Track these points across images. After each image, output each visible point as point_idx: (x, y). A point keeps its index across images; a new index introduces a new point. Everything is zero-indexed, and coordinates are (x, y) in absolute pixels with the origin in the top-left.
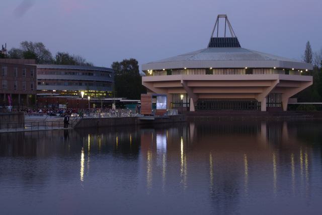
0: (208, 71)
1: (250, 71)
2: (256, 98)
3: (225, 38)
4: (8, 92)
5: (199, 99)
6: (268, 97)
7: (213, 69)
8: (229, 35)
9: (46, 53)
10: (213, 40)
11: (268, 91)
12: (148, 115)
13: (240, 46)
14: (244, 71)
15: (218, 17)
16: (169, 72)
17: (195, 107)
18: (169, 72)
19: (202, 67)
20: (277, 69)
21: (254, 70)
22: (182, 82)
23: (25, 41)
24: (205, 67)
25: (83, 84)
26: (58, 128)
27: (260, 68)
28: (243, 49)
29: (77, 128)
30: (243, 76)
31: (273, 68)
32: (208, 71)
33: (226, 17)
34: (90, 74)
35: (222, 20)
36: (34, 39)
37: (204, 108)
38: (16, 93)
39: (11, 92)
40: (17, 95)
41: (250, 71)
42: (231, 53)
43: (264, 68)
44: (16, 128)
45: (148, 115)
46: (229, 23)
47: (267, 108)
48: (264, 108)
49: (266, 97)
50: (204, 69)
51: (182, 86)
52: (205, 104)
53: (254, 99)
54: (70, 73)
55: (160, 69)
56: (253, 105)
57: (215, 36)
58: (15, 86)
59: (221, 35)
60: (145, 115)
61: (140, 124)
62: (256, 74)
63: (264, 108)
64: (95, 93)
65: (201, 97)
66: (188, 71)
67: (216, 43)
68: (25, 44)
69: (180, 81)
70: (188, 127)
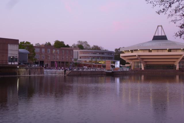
0: (150, 51)
1: (170, 50)
2: (174, 63)
3: (158, 36)
4: (60, 61)
5: (147, 64)
6: (180, 63)
7: (152, 50)
8: (163, 35)
9: (88, 45)
10: (154, 37)
11: (179, 61)
12: (109, 70)
13: (167, 39)
14: (167, 51)
15: (158, 27)
16: (132, 51)
17: (144, 68)
18: (132, 51)
19: (143, 49)
20: (183, 49)
21: (172, 50)
22: (137, 56)
23: (79, 40)
24: (148, 49)
25: (99, 58)
26: (58, 75)
27: (175, 49)
28: (170, 41)
29: (68, 75)
30: (147, 53)
31: (181, 49)
32: (150, 51)
33: (162, 26)
34: (102, 54)
35: (160, 28)
36: (83, 40)
37: (173, 68)
38: (63, 61)
39: (65, 61)
40: (64, 62)
41: (170, 50)
42: (162, 42)
43: (177, 49)
44: (39, 74)
45: (109, 70)
46: (163, 29)
47: (179, 68)
48: (177, 68)
49: (178, 63)
50: (147, 50)
51: (137, 58)
52: (173, 66)
53: (173, 64)
54: (94, 54)
55: (137, 49)
56: (173, 67)
57: (157, 35)
58: (63, 59)
59: (160, 35)
60: (108, 70)
61: (106, 74)
62: (173, 52)
63: (177, 68)
64: (105, 62)
65: (147, 63)
66: (140, 51)
67: (156, 38)
68: (79, 42)
69: (136, 56)
70: (141, 76)
